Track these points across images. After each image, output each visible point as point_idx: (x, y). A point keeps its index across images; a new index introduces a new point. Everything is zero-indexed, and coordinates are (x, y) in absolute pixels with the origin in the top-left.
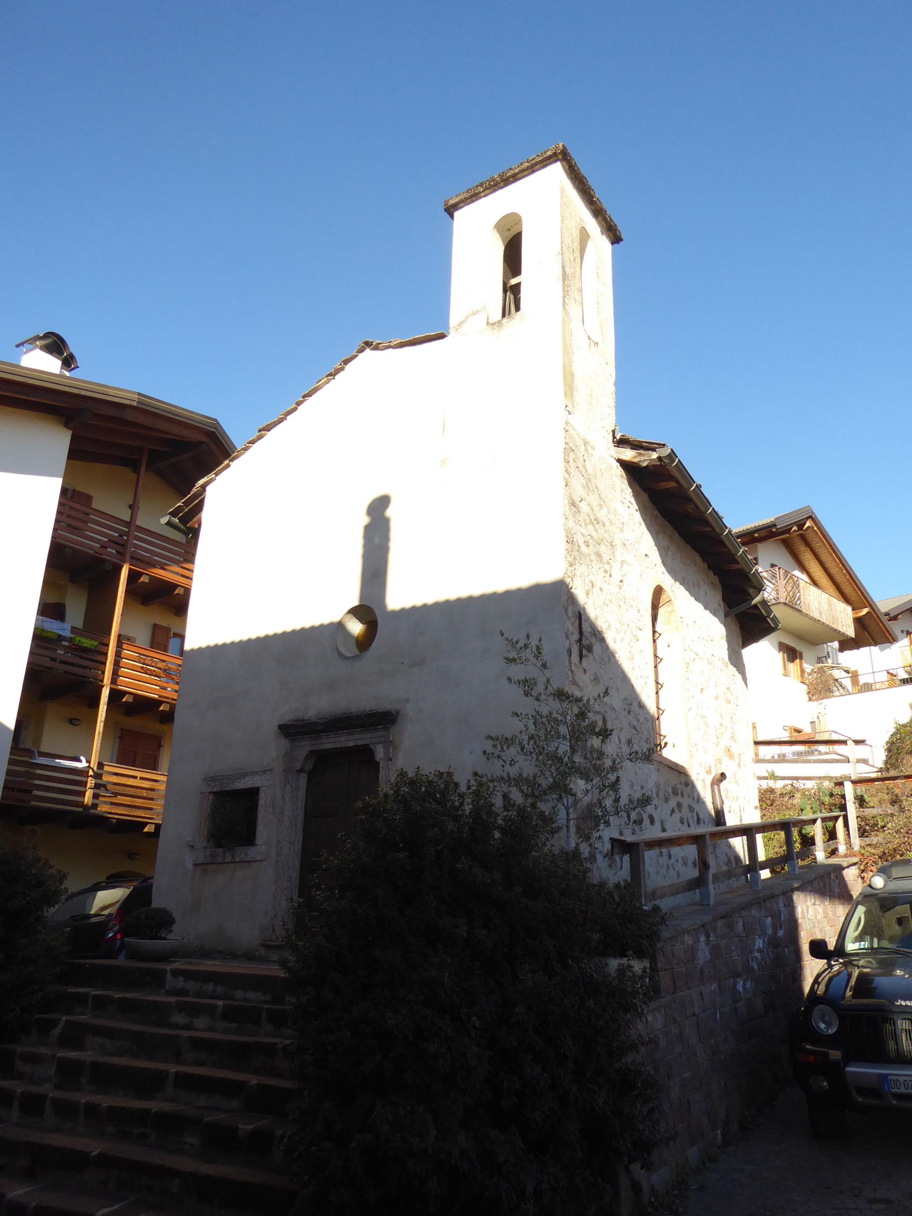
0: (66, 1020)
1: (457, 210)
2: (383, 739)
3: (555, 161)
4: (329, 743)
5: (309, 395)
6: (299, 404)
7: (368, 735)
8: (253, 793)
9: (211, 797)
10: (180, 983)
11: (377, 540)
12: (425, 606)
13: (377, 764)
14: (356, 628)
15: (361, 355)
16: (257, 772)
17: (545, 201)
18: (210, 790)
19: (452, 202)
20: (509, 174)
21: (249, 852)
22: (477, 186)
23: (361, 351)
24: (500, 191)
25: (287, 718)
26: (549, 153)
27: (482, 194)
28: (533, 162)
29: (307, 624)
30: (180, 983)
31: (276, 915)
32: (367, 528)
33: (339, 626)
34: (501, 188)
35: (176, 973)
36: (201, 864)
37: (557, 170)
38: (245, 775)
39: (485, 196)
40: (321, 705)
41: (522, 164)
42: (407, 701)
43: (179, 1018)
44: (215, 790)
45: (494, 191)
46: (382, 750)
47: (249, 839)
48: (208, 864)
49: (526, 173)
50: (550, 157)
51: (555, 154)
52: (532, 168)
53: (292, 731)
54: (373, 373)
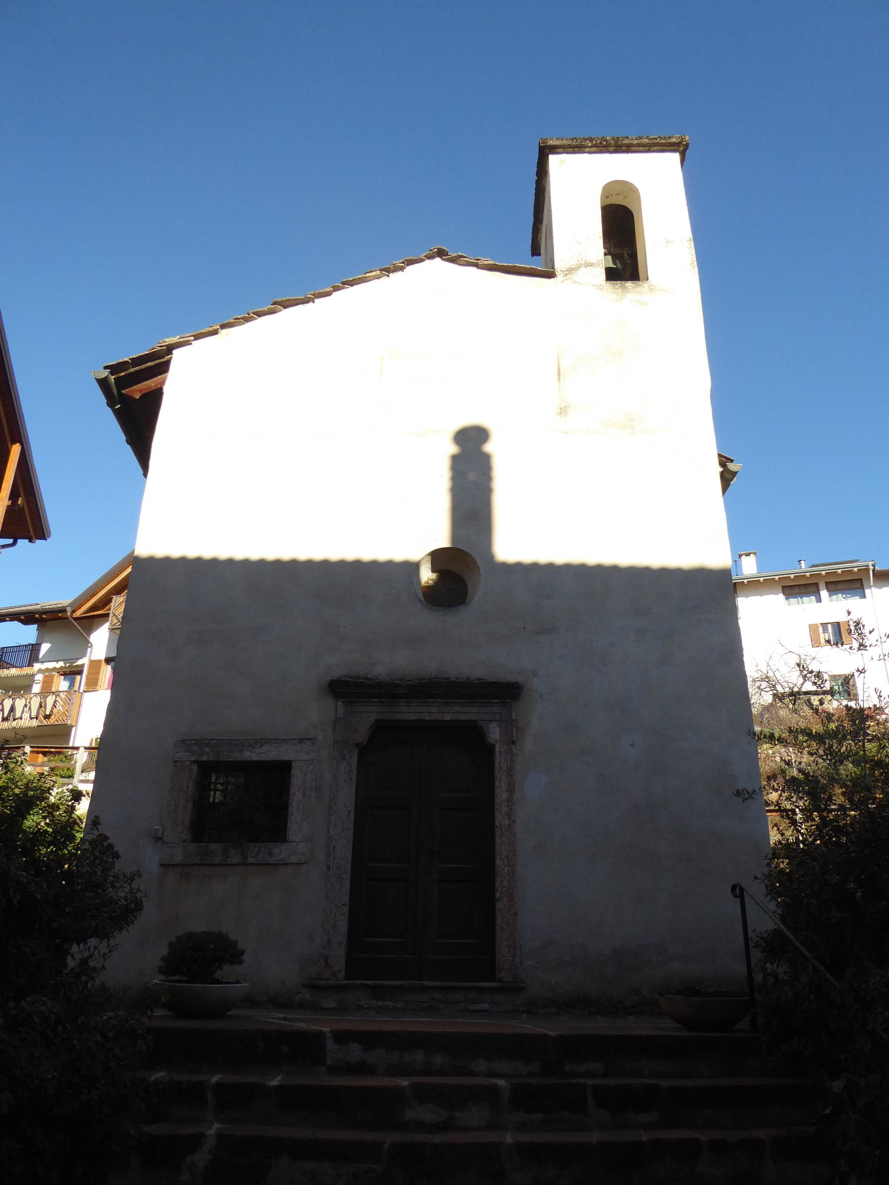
0: (219, 1136)
1: (553, 153)
2: (498, 717)
3: (675, 151)
4: (410, 712)
5: (351, 283)
6: (336, 289)
7: (475, 710)
8: (283, 768)
9: (195, 768)
10: (355, 1052)
11: (471, 476)
12: (550, 566)
13: (490, 751)
14: (427, 575)
15: (428, 262)
16: (285, 741)
17: (659, 184)
18: (193, 759)
19: (550, 143)
20: (624, 142)
21: (276, 851)
22: (585, 140)
23: (430, 257)
24: (607, 155)
25: (338, 672)
26: (674, 140)
27: (587, 150)
28: (655, 141)
29: (303, 555)
30: (355, 1052)
31: (329, 942)
32: (455, 459)
33: (413, 568)
34: (611, 152)
35: (342, 1037)
36: (177, 865)
37: (554, 160)
38: (263, 742)
39: (590, 153)
40: (390, 662)
41: (641, 138)
42: (534, 673)
43: (426, 1114)
44: (205, 758)
45: (601, 152)
46: (497, 730)
47: (278, 832)
48: (191, 865)
49: (641, 148)
50: (673, 144)
51: (678, 144)
52: (649, 148)
53: (345, 690)
54: (434, 287)
